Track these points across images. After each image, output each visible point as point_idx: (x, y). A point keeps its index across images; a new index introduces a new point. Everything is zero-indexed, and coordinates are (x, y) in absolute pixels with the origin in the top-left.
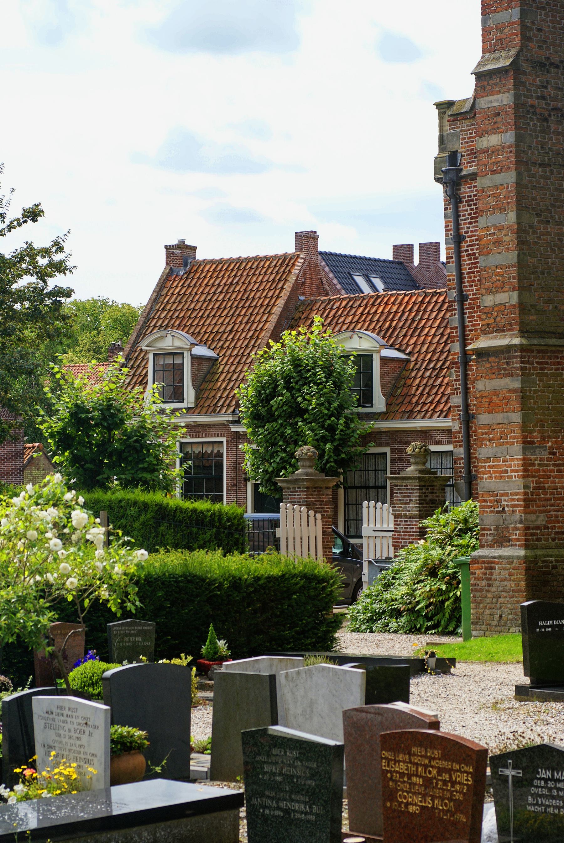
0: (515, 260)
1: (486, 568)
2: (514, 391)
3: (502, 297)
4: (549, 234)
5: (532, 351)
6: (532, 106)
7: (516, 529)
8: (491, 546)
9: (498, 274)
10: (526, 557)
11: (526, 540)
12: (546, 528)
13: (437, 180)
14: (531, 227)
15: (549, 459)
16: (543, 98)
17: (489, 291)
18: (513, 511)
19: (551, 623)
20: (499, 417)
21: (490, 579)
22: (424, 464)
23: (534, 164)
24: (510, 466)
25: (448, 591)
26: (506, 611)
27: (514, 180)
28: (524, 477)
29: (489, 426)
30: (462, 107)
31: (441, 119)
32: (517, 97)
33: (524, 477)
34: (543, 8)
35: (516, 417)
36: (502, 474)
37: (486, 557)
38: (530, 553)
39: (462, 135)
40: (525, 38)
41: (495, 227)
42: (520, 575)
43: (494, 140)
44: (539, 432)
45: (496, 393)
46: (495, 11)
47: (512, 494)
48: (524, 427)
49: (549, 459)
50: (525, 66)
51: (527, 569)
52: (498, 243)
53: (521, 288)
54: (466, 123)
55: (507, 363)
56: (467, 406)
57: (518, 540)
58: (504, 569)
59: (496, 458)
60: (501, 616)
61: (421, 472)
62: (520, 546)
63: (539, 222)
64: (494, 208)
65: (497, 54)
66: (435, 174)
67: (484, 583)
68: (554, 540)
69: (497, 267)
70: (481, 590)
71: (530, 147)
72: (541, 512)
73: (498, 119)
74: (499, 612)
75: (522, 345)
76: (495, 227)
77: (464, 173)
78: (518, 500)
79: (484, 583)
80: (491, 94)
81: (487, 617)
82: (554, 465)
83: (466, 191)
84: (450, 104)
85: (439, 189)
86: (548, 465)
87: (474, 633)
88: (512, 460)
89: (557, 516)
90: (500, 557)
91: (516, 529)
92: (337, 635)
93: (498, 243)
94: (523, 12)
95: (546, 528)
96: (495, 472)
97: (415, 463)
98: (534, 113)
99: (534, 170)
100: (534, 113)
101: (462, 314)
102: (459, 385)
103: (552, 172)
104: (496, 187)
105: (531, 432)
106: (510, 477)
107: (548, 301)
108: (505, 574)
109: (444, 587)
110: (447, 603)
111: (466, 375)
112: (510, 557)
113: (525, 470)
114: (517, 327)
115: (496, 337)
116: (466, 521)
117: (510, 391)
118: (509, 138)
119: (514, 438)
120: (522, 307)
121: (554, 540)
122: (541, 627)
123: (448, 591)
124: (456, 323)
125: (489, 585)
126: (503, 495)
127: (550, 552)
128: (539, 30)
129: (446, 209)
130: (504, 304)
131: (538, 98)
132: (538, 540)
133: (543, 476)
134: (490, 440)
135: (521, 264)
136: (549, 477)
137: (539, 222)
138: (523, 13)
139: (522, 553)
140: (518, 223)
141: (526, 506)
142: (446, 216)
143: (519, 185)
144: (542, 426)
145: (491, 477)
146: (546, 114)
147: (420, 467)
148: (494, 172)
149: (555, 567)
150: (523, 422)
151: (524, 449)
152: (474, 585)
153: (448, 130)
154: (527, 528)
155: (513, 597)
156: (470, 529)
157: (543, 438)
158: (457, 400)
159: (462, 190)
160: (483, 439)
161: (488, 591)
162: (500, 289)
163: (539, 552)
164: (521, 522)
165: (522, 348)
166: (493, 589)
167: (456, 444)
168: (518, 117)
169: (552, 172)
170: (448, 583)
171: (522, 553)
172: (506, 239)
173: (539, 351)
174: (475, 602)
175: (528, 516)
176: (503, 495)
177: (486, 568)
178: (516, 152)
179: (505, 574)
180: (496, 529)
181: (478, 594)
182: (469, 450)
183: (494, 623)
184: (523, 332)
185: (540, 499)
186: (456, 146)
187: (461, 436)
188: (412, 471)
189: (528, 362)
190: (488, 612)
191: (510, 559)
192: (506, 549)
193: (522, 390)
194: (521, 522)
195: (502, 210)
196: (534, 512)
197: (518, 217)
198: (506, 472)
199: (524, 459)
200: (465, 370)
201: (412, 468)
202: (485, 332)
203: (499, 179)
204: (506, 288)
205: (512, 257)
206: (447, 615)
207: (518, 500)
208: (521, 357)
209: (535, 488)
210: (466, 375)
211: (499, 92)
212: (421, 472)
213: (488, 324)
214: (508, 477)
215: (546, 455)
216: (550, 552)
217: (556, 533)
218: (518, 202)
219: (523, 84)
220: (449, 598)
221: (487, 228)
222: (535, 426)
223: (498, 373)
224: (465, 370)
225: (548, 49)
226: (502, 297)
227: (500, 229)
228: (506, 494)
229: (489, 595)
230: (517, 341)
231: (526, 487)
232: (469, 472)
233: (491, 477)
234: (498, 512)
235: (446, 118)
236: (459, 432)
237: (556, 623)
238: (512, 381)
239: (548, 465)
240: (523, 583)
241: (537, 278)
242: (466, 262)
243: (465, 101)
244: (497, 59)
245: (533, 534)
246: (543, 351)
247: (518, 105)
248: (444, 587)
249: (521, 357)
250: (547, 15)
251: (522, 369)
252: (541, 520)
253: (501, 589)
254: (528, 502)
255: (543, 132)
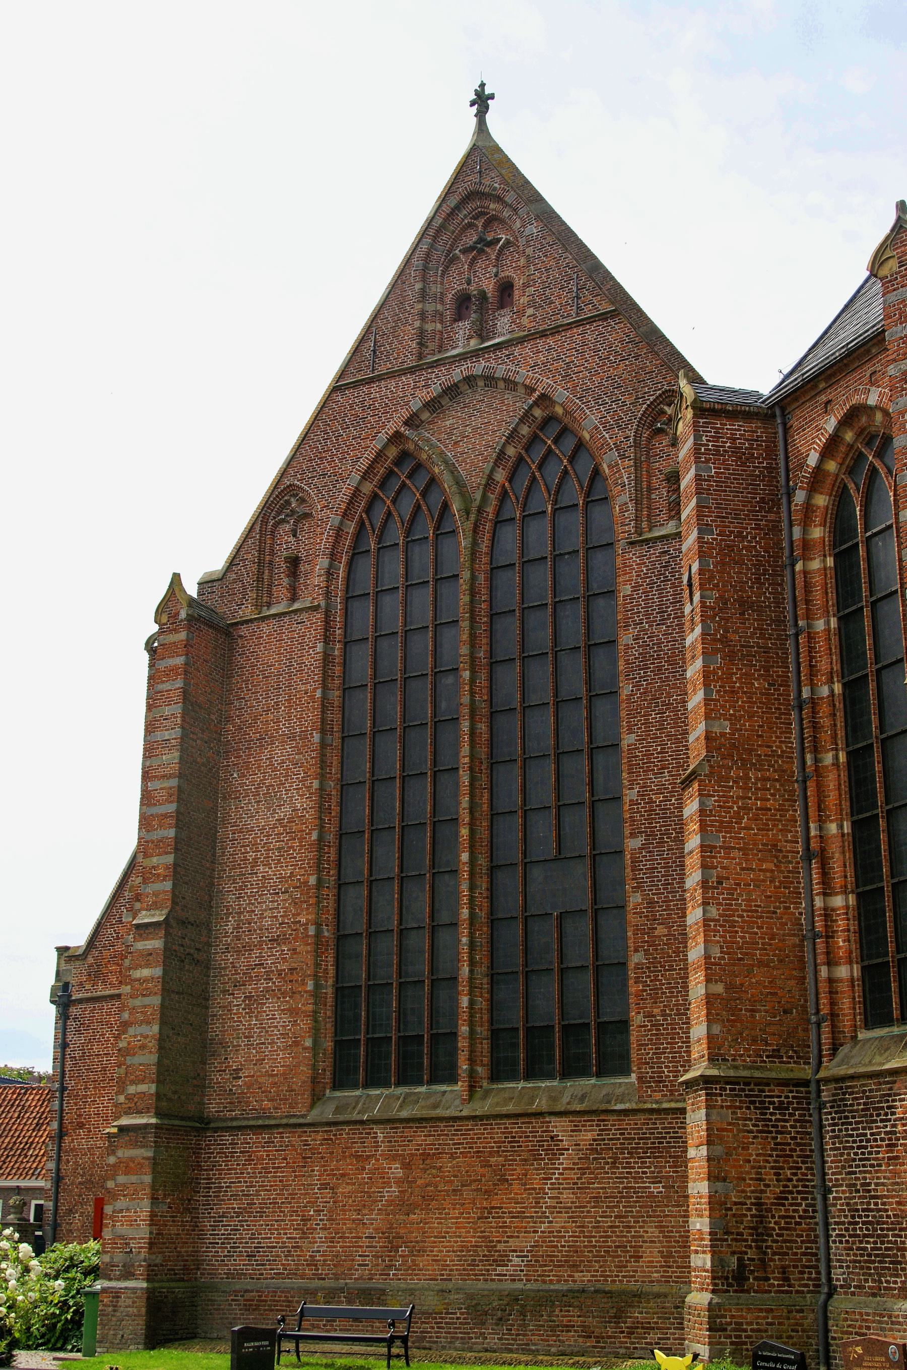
0: (156, 1060)
1: (113, 1297)
2: (148, 1158)
3: (142, 1088)
4: (178, 1043)
5: (162, 1129)
6: (175, 951)
7: (141, 1266)
8: (119, 1280)
9: (141, 1070)
10: (147, 1288)
11: (148, 1275)
12: (162, 1265)
13: (52, 1002)
14: (168, 1037)
15: (168, 1212)
16: (182, 945)
17: (133, 1082)
18: (139, 1252)
19: (252, 1344)
20: (134, 1178)
21: (116, 1306)
22: (21, 1213)
23: (173, 991)
24: (139, 1216)
25: (60, 1315)
26: (128, 1332)
27: (159, 1002)
28: (150, 1225)
29: (124, 1185)
30: (76, 951)
31: (59, 959)
32: (166, 943)
33: (150, 1225)
34: (186, 883)
35: (148, 1179)
36: (132, 1223)
37: (112, 1288)
38: (151, 1286)
39: (74, 971)
40: (174, 903)
41: (142, 1035)
42: (142, 1303)
43: (146, 972)
44: (163, 1190)
45: (132, 1159)
46: (153, 882)
47: (139, 1239)
48: (153, 1187)
49: (168, 1212)
50: (173, 922)
51: (148, 1298)
52: (143, 1047)
53: (159, 1082)
54: (78, 963)
55: (144, 1137)
56: (58, 1170)
57: (141, 1275)
58: (129, 1298)
59: (128, 1210)
60: (123, 1336)
61: (19, 1219)
62: (143, 1279)
63: (174, 1034)
64: (142, 1022)
65: (153, 912)
66: (51, 997)
67: (111, 1309)
68: (166, 1275)
69: (140, 1065)
70: (107, 1315)
71: (171, 979)
72: (160, 1253)
73: (151, 958)
74: (121, 1333)
75: (157, 1124)
76: (142, 1035)
77: (73, 998)
78: (144, 1244)
79: (111, 1309)
80: (147, 939)
81: (110, 1337)
82: (171, 1217)
83: (74, 1011)
84: (67, 949)
85: (53, 1007)
86: (166, 1217)
87: (98, 1350)
88: (142, 1212)
89: (169, 1256)
90: (126, 1288)
91: (141, 1266)
92: (14, 1353)
93: (143, 1047)
94: (174, 884)
95: (162, 1265)
96: (126, 1221)
97: (15, 1213)
98: (176, 956)
99: (173, 996)
100: (176, 956)
101: (62, 1100)
102: (54, 1154)
103: (184, 998)
104: (145, 1007)
105: (157, 1190)
106: (139, 1225)
107: (175, 1092)
108: (129, 1302)
109: (58, 1312)
110: (59, 1325)
111: (60, 1147)
112: (134, 1288)
113: (151, 1220)
114: (153, 1110)
115: (135, 1117)
116: (71, 1258)
117: (144, 1158)
118: (158, 972)
119: (145, 1194)
120: (158, 1096)
121: (166, 1275)
122: (245, 1348)
123: (60, 1315)
124: (57, 1108)
125: (115, 1311)
126: (131, 1239)
127: (164, 1284)
128: (183, 898)
129: (56, 1023)
130: (144, 1093)
131: (179, 945)
132: (156, 1275)
133: (163, 1225)
134: (124, 1196)
135: (159, 1064)
136: (166, 1225)
137: (174, 1034)
138: (174, 885)
139: (145, 1285)
140: (160, 1034)
141: (150, 1248)
142: (56, 1028)
143: (163, 1006)
144: (165, 1186)
145: (122, 1225)
146: (183, 957)
147: (18, 1216)
148: (144, 995)
149: (166, 1297)
150: (153, 1182)
151: (152, 1203)
152: (102, 1310)
153: (63, 967)
154: (149, 1266)
155: (134, 1320)
156: (77, 1266)
157: (165, 1195)
158: (52, 1165)
159: (71, 1010)
160: (119, 1195)
161: (113, 1316)
162: (142, 1081)
163: (157, 1285)
164: (145, 1260)
165: (156, 1126)
166: (118, 1314)
167: (47, 1199)
168: (166, 957)
169: (184, 998)
170: (61, 1308)
171: (145, 1285)
172: (150, 1044)
173: (167, 1129)
174: (101, 1324)
175: (151, 1256)
176: (131, 1239)
177: (113, 1297)
178: (163, 982)
179: (129, 1302)
180: (124, 1266)
181: (104, 1318)
182: (57, 1203)
183: (118, 1341)
184: (158, 1115)
185: (159, 1243)
186: (69, 979)
187: (52, 1193)
188: (12, 1219)
189: (159, 1137)
190: (112, 1332)
191: (134, 1290)
192: (131, 1282)
193: (154, 1158)
194: (145, 1260)
195: (148, 1023)
196: (154, 1253)
197: (160, 1029)
198: (136, 1221)
199: (151, 1212)
200: (60, 1143)
201: (12, 1216)
202: (126, 1113)
203: (147, 1001)
204: (147, 1081)
205: (153, 1058)
206: (57, 1334)
207: (144, 1243)
208: (156, 1133)
209: (157, 1234)
210: (60, 1147)
211: (153, 939)
212: (19, 1219)
213: (129, 1108)
214: (137, 1225)
215: (165, 1208)
216: (164, 1284)
217: (168, 1270)
218: (161, 1018)
219: (170, 934)
220: (61, 1320)
221: (135, 1036)
222: (160, 1186)
223: (135, 1145)
224: (60, 1143)
225: (188, 912)
226: (142, 1088)
227: (146, 1037)
228: (135, 1239)
229: (114, 1319)
230: (153, 1121)
231: (151, 1233)
232: (55, 1220)
233: (122, 1225)
234: (126, 1252)
235: (63, 958)
236: (50, 1190)
237: (257, 1344)
238: (147, 1151)
239: (166, 1217)
240: (144, 1310)
241: (170, 1075)
242: (69, 1063)
243: (79, 947)
244: (153, 915)
245: (153, 1270)
246: (171, 1129)
247: (166, 948)
248: (58, 1312)
249: (156, 1133)
250: (188, 889)
251: (155, 1142)
252: (159, 1260)
253: (124, 1314)
254: (151, 1244)
255: (181, 969)
